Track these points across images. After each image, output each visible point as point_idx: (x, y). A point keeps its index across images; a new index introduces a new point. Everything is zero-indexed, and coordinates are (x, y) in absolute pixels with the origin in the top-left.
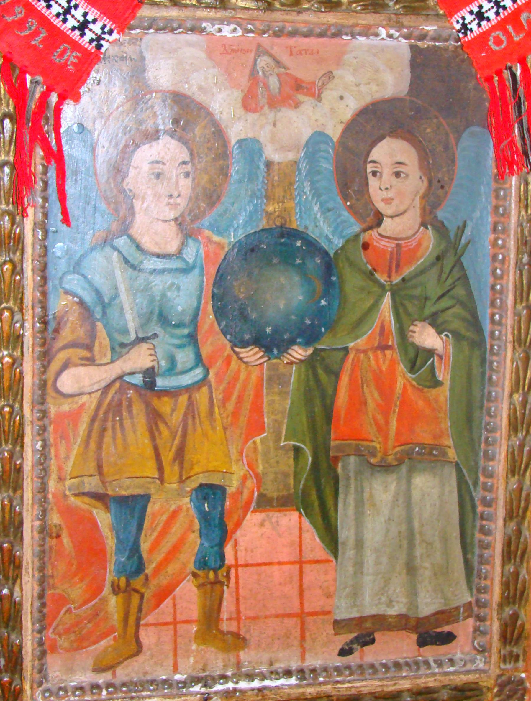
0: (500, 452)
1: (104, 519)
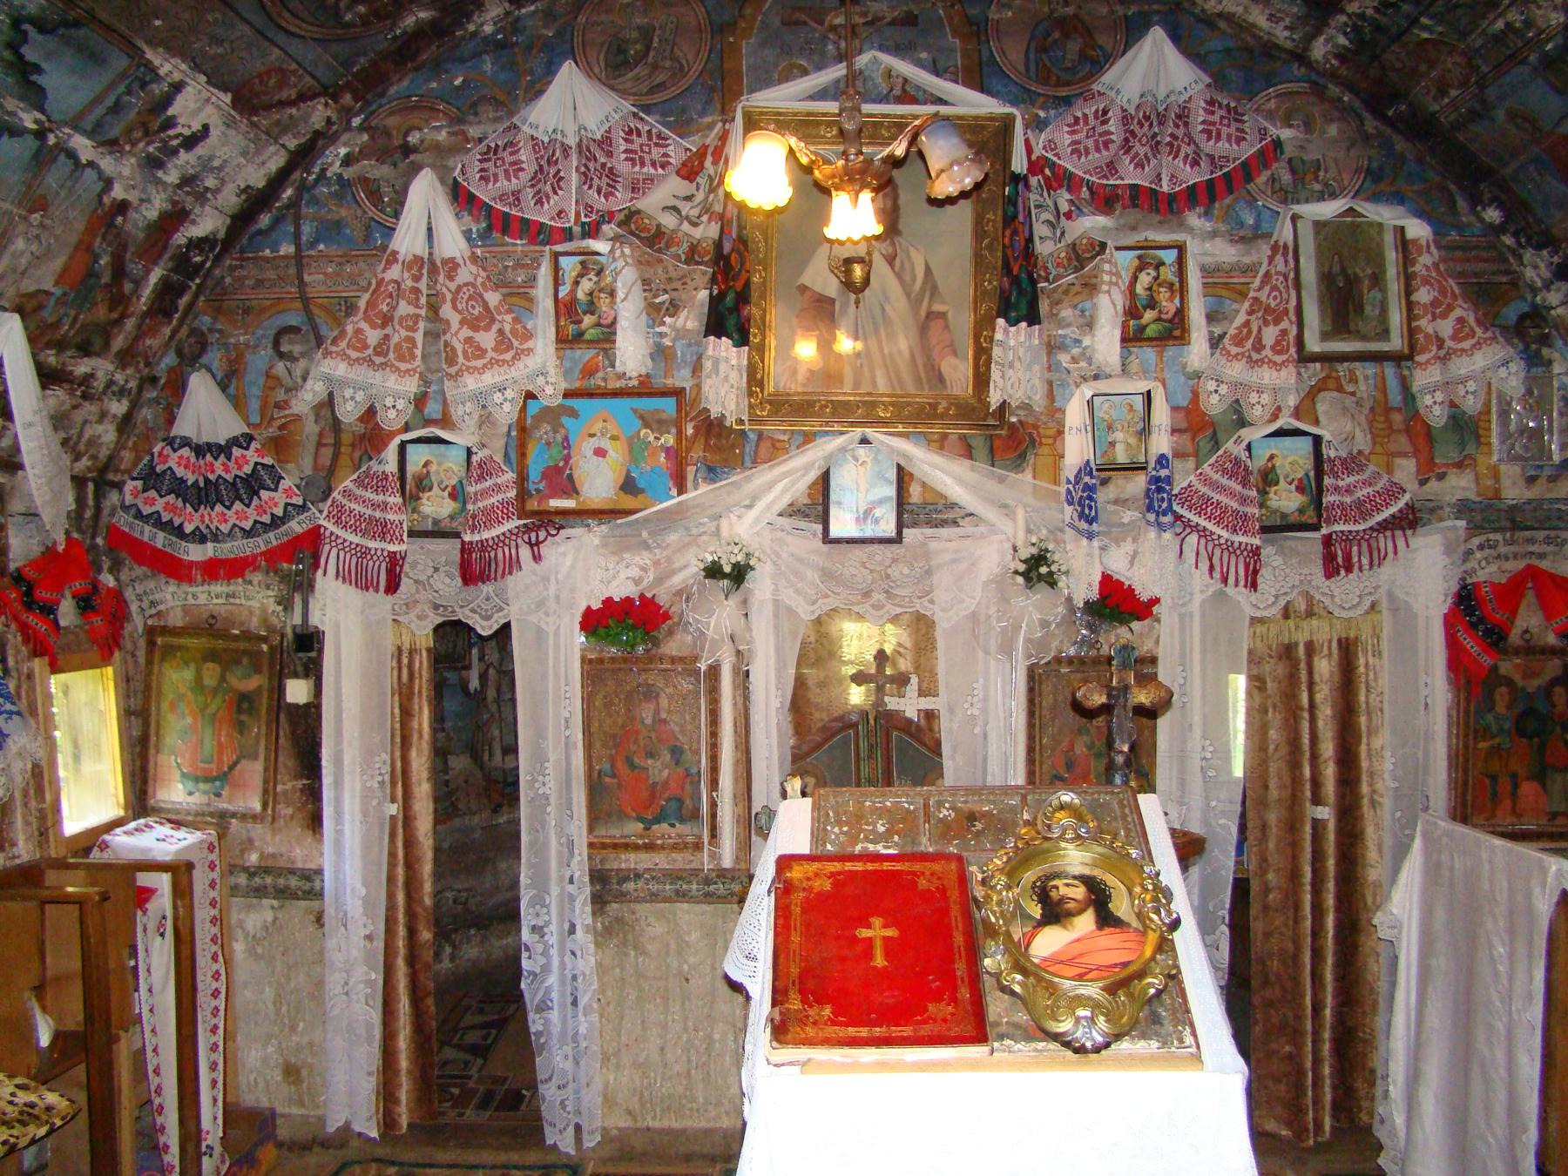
0: (1312, 705)
1: (1487, 781)
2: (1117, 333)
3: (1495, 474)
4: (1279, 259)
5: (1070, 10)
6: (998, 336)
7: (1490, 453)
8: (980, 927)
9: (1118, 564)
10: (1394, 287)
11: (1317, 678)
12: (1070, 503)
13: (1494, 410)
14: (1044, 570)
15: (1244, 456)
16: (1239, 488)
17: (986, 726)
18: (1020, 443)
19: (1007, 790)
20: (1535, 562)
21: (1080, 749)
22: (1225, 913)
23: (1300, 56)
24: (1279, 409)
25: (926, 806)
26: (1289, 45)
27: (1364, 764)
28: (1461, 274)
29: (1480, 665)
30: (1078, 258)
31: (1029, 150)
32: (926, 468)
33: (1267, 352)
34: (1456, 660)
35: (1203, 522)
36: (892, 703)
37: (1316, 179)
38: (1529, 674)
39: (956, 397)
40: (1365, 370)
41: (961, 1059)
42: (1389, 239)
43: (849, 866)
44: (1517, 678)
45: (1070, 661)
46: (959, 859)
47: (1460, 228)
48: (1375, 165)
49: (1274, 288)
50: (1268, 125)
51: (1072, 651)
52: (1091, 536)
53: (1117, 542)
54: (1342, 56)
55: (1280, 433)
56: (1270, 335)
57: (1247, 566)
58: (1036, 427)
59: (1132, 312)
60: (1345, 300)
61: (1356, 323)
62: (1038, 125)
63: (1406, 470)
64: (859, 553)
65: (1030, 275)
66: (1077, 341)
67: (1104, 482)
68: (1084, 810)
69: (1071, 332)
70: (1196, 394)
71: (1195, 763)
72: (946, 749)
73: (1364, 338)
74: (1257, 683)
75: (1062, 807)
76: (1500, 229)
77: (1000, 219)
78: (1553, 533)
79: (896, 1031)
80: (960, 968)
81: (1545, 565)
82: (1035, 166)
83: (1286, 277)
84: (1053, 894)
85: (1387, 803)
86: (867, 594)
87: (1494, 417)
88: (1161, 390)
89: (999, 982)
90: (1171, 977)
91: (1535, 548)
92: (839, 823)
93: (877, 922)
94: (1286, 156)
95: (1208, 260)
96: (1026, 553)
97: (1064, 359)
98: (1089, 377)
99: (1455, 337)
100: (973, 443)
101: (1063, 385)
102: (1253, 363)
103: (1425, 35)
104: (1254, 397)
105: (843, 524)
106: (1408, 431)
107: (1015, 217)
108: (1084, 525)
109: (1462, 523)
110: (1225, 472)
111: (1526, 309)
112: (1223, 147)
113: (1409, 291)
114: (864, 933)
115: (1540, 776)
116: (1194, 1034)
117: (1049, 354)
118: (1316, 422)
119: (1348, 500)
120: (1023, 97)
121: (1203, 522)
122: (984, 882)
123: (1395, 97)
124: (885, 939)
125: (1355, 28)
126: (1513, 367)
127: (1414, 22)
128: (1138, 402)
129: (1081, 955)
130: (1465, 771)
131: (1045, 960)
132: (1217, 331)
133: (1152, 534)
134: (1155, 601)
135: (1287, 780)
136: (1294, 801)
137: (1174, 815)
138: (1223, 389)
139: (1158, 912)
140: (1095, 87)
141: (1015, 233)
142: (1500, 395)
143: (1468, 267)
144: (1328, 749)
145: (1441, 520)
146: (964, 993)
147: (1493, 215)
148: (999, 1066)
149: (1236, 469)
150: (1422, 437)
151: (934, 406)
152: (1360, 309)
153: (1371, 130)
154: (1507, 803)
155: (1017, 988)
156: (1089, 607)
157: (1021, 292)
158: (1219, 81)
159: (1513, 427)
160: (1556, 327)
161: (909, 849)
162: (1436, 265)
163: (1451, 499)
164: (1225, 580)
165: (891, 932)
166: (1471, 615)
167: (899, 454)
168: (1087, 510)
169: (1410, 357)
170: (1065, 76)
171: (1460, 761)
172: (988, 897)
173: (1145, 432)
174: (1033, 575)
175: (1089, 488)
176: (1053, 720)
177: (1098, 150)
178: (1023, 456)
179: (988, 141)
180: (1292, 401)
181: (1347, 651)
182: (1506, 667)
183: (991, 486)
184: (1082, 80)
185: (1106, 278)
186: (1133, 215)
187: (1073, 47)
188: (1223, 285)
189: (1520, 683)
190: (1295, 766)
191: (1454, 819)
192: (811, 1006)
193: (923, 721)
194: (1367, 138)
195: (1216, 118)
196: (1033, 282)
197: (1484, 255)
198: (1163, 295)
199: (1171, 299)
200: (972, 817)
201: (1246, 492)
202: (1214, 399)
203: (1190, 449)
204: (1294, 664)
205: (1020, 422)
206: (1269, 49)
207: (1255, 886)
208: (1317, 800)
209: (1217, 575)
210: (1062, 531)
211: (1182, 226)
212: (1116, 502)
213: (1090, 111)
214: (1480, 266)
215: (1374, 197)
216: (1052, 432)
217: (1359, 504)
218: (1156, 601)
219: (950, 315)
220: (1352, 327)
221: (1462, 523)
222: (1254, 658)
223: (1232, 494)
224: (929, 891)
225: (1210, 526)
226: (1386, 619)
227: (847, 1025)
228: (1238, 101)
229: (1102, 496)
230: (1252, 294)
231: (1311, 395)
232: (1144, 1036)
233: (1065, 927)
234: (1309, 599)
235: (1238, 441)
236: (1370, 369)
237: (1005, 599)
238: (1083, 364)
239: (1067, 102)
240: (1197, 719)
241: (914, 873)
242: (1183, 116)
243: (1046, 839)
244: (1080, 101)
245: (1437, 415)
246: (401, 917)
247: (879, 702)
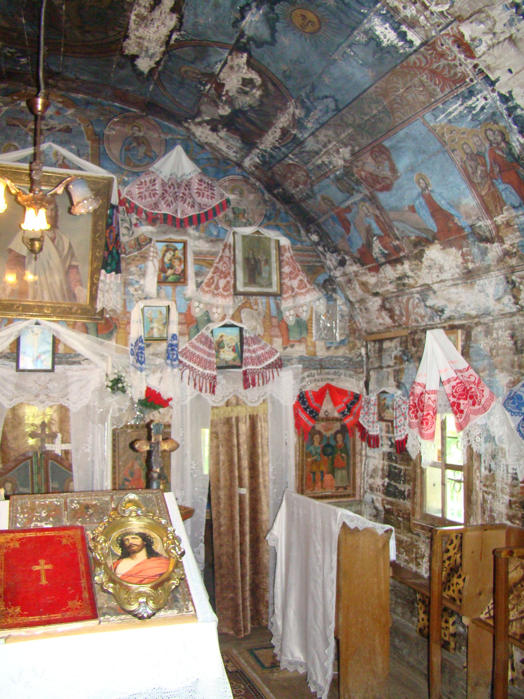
1: (311, 475)
2: (156, 279)
3: (314, 346)
4: (227, 250)
5: (141, 134)
6: (102, 278)
7: (312, 337)
8: (92, 561)
9: (154, 382)
10: (274, 265)
11: (241, 432)
12: (132, 355)
13: (314, 319)
14: (120, 385)
15: (210, 335)
16: (207, 349)
17: (94, 459)
18: (110, 327)
19: (103, 492)
20: (330, 382)
21: (137, 467)
22: (202, 538)
23: (239, 165)
24: (225, 315)
25: (66, 503)
26: (235, 159)
27: (261, 469)
28: (302, 262)
29: (307, 425)
30: (139, 244)
31: (120, 195)
32: (66, 337)
33: (221, 290)
34: (299, 423)
35: (192, 364)
36: (49, 447)
37: (244, 217)
38: (327, 430)
39: (81, 305)
40: (262, 300)
41: (85, 627)
42: (273, 245)
43: (28, 535)
44: (322, 431)
45: (132, 426)
46: (82, 528)
47: (302, 242)
48: (268, 213)
49: (225, 263)
50: (223, 192)
51: (133, 422)
52: (141, 370)
53: (154, 372)
54: (256, 166)
55: (225, 326)
56: (222, 283)
57: (210, 384)
58: (118, 320)
59: (163, 270)
60: (254, 270)
61: (258, 280)
62: (124, 184)
63: (278, 343)
64: (34, 376)
65: (117, 252)
66: (138, 282)
67: (148, 346)
68: (140, 502)
69: (135, 278)
70: (189, 308)
71: (188, 472)
72: (74, 468)
73: (262, 286)
74: (214, 435)
75: (130, 501)
76: (318, 244)
77: (105, 224)
78: (337, 370)
79: (53, 616)
80: (84, 583)
81: (333, 384)
82: (122, 202)
83: (229, 258)
84: (127, 543)
85: (271, 486)
86: (37, 396)
87: (314, 322)
88: (174, 305)
89: (102, 587)
90: (181, 579)
91: (330, 377)
92: (23, 513)
93: (42, 562)
94: (231, 207)
95: (197, 249)
96: (112, 378)
97: (131, 289)
98: (142, 298)
99: (299, 287)
100: (89, 326)
101: (131, 301)
102: (214, 295)
103: (291, 162)
104: (214, 310)
105: (26, 363)
106: (279, 326)
107: (112, 224)
108: (139, 365)
109: (300, 366)
110: (201, 342)
111: (327, 277)
112: (204, 200)
113: (280, 267)
114: (36, 568)
115: (332, 472)
116: (193, 605)
117: (125, 287)
118: (241, 322)
119: (254, 355)
120: (118, 170)
121: (192, 364)
122: (93, 539)
123: (278, 185)
124: (47, 571)
125: (263, 156)
126: (322, 301)
127: (286, 156)
128: (164, 310)
129: (141, 571)
130: (303, 470)
131: (123, 575)
132: (200, 280)
133: (169, 369)
134: (170, 399)
135: (228, 477)
136: (231, 486)
137: (180, 500)
138: (202, 306)
139: (175, 549)
140: (151, 169)
141: (111, 231)
142: (316, 312)
143: (305, 258)
144: (245, 463)
145: (292, 364)
146: (86, 595)
147: (315, 238)
148: (104, 629)
149: (207, 342)
150: (285, 329)
151: (70, 309)
152: (260, 273)
153: (267, 199)
155: (111, 590)
156: (141, 402)
157: (113, 258)
158: (204, 172)
159: (321, 326)
160: (338, 285)
161: (58, 525)
162: (292, 257)
163: (296, 355)
164: (201, 390)
165: (49, 567)
166: (304, 404)
167: (54, 330)
168: (139, 358)
169: (280, 295)
170: (137, 163)
171: (301, 466)
172: (95, 546)
173: (167, 323)
174: (115, 387)
175: (140, 348)
176: (124, 453)
177: (150, 197)
178: (111, 333)
179: (101, 190)
180: (231, 312)
181: (253, 421)
182: (319, 426)
183: (96, 346)
184: (145, 165)
185: (151, 254)
186: (165, 227)
187: (142, 150)
188: (202, 260)
189: (324, 433)
190: (231, 471)
191: (298, 492)
192: (10, 608)
193: (64, 455)
194: (265, 202)
195: (202, 188)
196: (118, 254)
197: (311, 254)
198: (176, 263)
199: (180, 265)
200: (87, 507)
201: (210, 351)
202: (197, 310)
203: (186, 331)
204: (231, 427)
205: (111, 318)
206: (226, 160)
207: (215, 525)
208: (241, 486)
209: (198, 387)
210: (128, 367)
211: (186, 233)
212: (153, 354)
213: (148, 179)
214: (309, 259)
215: (268, 227)
216: (125, 322)
217: (259, 357)
218: (170, 399)
219: (80, 267)
220: (257, 281)
221: (300, 366)
222: (213, 424)
223: (205, 352)
224: (67, 545)
225: (195, 366)
226: (270, 405)
227: (28, 615)
228: (212, 180)
229: (147, 352)
230: (215, 265)
231: (239, 310)
232: (171, 608)
233: (132, 558)
234: (237, 399)
235: (207, 329)
236: (264, 300)
237: (102, 398)
238: (140, 292)
239: (137, 174)
240: (189, 452)
241: (60, 537)
242: (188, 185)
243: (123, 517)
244: (144, 175)
245: (291, 320)
247: (42, 447)
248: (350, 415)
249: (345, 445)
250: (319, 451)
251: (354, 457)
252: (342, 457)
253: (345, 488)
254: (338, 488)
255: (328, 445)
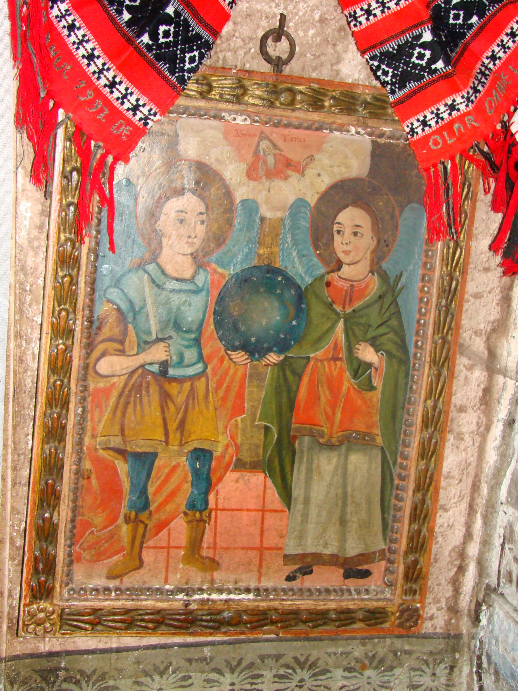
1: (122, 468)
130: (54, 433)
154: (180, 529)
246: (10, 443)
248: (449, 83)
249: (391, 291)
250: (194, 309)
251: (444, 363)
252: (360, 369)
253: (355, 569)
254: (305, 565)
255: (266, 278)
